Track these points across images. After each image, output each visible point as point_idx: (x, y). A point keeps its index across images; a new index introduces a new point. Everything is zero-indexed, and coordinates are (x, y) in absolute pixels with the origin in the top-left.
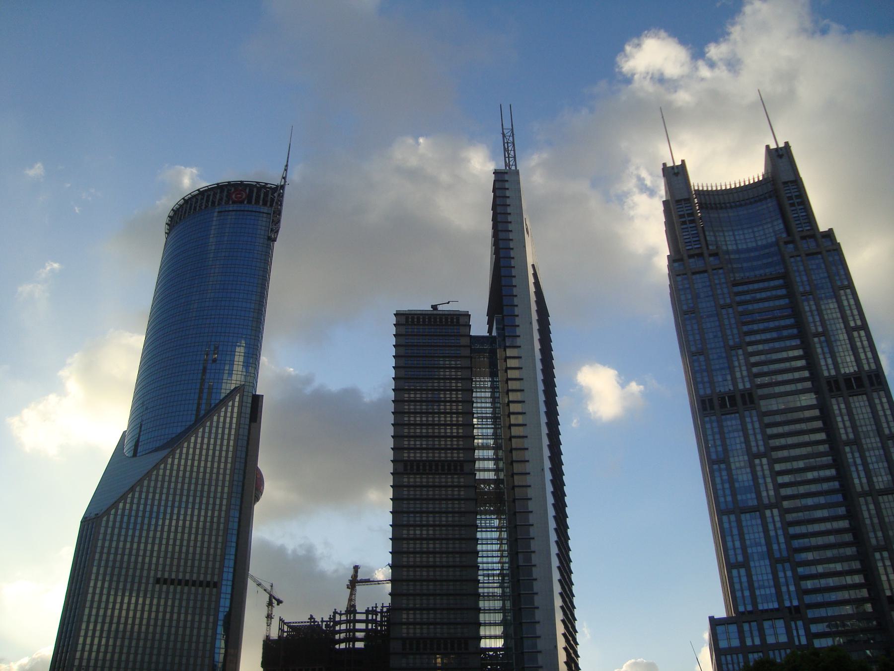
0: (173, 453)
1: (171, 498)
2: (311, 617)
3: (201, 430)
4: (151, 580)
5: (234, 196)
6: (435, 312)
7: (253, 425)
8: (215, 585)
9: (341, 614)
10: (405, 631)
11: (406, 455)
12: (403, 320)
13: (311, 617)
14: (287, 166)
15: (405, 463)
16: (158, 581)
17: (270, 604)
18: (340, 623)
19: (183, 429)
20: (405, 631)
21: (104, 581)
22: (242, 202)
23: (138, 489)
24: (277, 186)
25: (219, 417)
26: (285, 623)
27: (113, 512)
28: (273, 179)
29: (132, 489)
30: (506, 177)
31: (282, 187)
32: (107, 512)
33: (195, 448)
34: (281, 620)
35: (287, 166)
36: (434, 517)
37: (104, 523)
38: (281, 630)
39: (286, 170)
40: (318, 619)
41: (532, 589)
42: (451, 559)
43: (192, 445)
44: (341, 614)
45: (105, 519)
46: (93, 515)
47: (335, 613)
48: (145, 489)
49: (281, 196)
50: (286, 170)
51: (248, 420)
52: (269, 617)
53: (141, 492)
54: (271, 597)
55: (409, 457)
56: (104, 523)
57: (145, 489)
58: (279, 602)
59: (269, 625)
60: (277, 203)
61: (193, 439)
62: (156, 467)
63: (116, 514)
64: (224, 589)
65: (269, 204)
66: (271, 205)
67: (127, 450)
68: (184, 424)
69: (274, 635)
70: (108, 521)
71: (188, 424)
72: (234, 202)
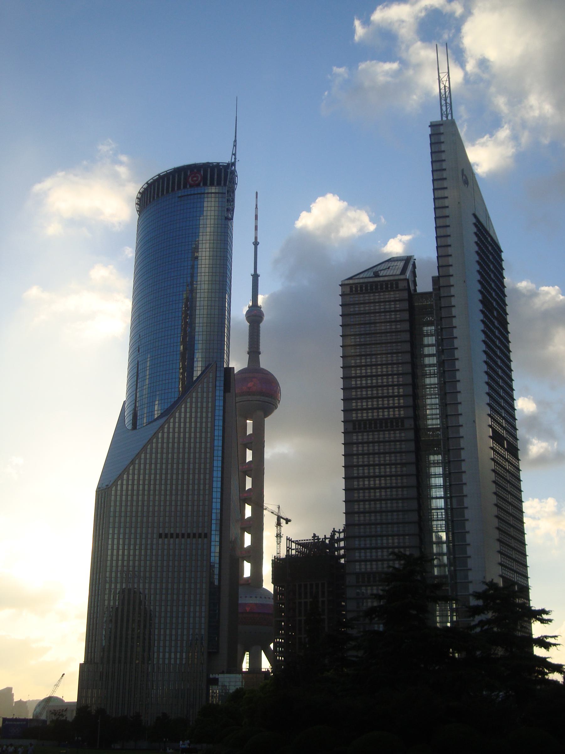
0: (168, 421)
1: (193, 424)
2: (315, 536)
3: (183, 406)
4: (155, 536)
5: (190, 179)
6: (376, 279)
7: (227, 394)
8: (206, 536)
9: (339, 533)
10: (357, 567)
11: (354, 415)
12: (347, 290)
13: (315, 536)
14: (235, 141)
15: (354, 422)
16: (160, 536)
17: (279, 524)
18: (339, 540)
19: (169, 405)
20: (357, 567)
21: (119, 539)
22: (198, 185)
23: (137, 462)
24: (228, 164)
25: (180, 413)
26: (293, 542)
27: (119, 482)
28: (224, 158)
29: (132, 462)
30: (442, 129)
31: (233, 164)
32: (115, 483)
33: (180, 422)
34: (288, 539)
35: (235, 141)
36: (396, 456)
37: (113, 492)
38: (289, 549)
39: (235, 146)
40: (321, 537)
41: (464, 528)
42: (395, 505)
43: (177, 420)
44: (339, 533)
45: (114, 489)
46: (104, 486)
47: (334, 531)
48: (142, 461)
49: (233, 173)
50: (235, 146)
51: (222, 393)
52: (279, 536)
53: (140, 464)
54: (279, 518)
55: (357, 417)
56: (113, 492)
57: (142, 461)
58: (288, 521)
59: (279, 543)
60: (230, 182)
61: (177, 414)
62: (156, 435)
63: (122, 485)
64: (213, 538)
65: (222, 182)
66: (225, 184)
67: (128, 420)
68: (169, 400)
69: (283, 554)
70: (116, 490)
71: (173, 400)
72: (191, 186)
